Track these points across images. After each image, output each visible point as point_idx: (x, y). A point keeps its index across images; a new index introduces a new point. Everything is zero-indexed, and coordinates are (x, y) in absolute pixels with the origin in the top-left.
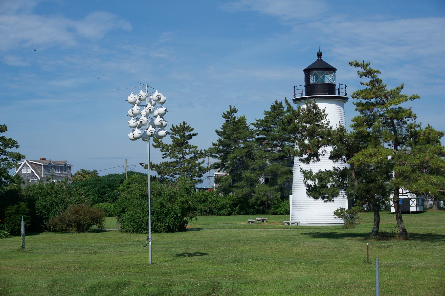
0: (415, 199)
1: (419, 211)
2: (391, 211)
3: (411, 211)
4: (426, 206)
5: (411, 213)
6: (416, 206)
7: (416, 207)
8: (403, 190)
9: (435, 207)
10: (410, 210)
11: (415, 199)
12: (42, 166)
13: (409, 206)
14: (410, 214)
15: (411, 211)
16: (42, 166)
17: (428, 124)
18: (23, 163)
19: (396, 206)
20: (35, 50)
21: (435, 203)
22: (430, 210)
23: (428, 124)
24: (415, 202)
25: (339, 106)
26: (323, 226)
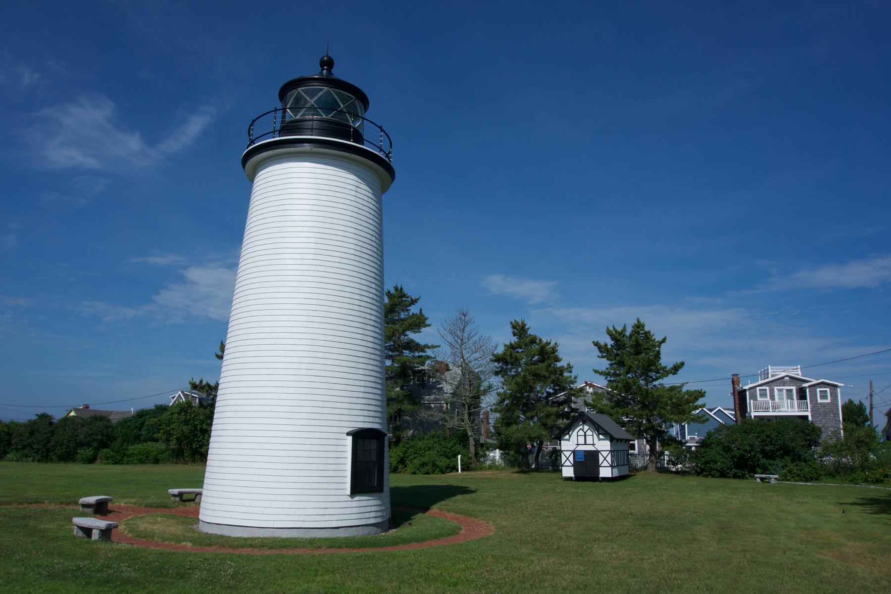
0: (564, 465)
1: (617, 476)
2: (564, 475)
3: (601, 475)
4: (636, 465)
5: (600, 480)
6: (612, 466)
7: (610, 468)
8: (585, 433)
9: (651, 468)
10: (599, 474)
11: (564, 465)
12: (197, 399)
13: (597, 466)
14: (600, 482)
15: (601, 475)
16: (197, 399)
17: (638, 319)
18: (177, 395)
19: (737, 409)
20: (843, 512)
21: (651, 459)
22: (642, 472)
23: (638, 319)
24: (609, 459)
25: (352, 177)
26: (274, 540)
